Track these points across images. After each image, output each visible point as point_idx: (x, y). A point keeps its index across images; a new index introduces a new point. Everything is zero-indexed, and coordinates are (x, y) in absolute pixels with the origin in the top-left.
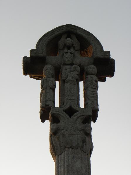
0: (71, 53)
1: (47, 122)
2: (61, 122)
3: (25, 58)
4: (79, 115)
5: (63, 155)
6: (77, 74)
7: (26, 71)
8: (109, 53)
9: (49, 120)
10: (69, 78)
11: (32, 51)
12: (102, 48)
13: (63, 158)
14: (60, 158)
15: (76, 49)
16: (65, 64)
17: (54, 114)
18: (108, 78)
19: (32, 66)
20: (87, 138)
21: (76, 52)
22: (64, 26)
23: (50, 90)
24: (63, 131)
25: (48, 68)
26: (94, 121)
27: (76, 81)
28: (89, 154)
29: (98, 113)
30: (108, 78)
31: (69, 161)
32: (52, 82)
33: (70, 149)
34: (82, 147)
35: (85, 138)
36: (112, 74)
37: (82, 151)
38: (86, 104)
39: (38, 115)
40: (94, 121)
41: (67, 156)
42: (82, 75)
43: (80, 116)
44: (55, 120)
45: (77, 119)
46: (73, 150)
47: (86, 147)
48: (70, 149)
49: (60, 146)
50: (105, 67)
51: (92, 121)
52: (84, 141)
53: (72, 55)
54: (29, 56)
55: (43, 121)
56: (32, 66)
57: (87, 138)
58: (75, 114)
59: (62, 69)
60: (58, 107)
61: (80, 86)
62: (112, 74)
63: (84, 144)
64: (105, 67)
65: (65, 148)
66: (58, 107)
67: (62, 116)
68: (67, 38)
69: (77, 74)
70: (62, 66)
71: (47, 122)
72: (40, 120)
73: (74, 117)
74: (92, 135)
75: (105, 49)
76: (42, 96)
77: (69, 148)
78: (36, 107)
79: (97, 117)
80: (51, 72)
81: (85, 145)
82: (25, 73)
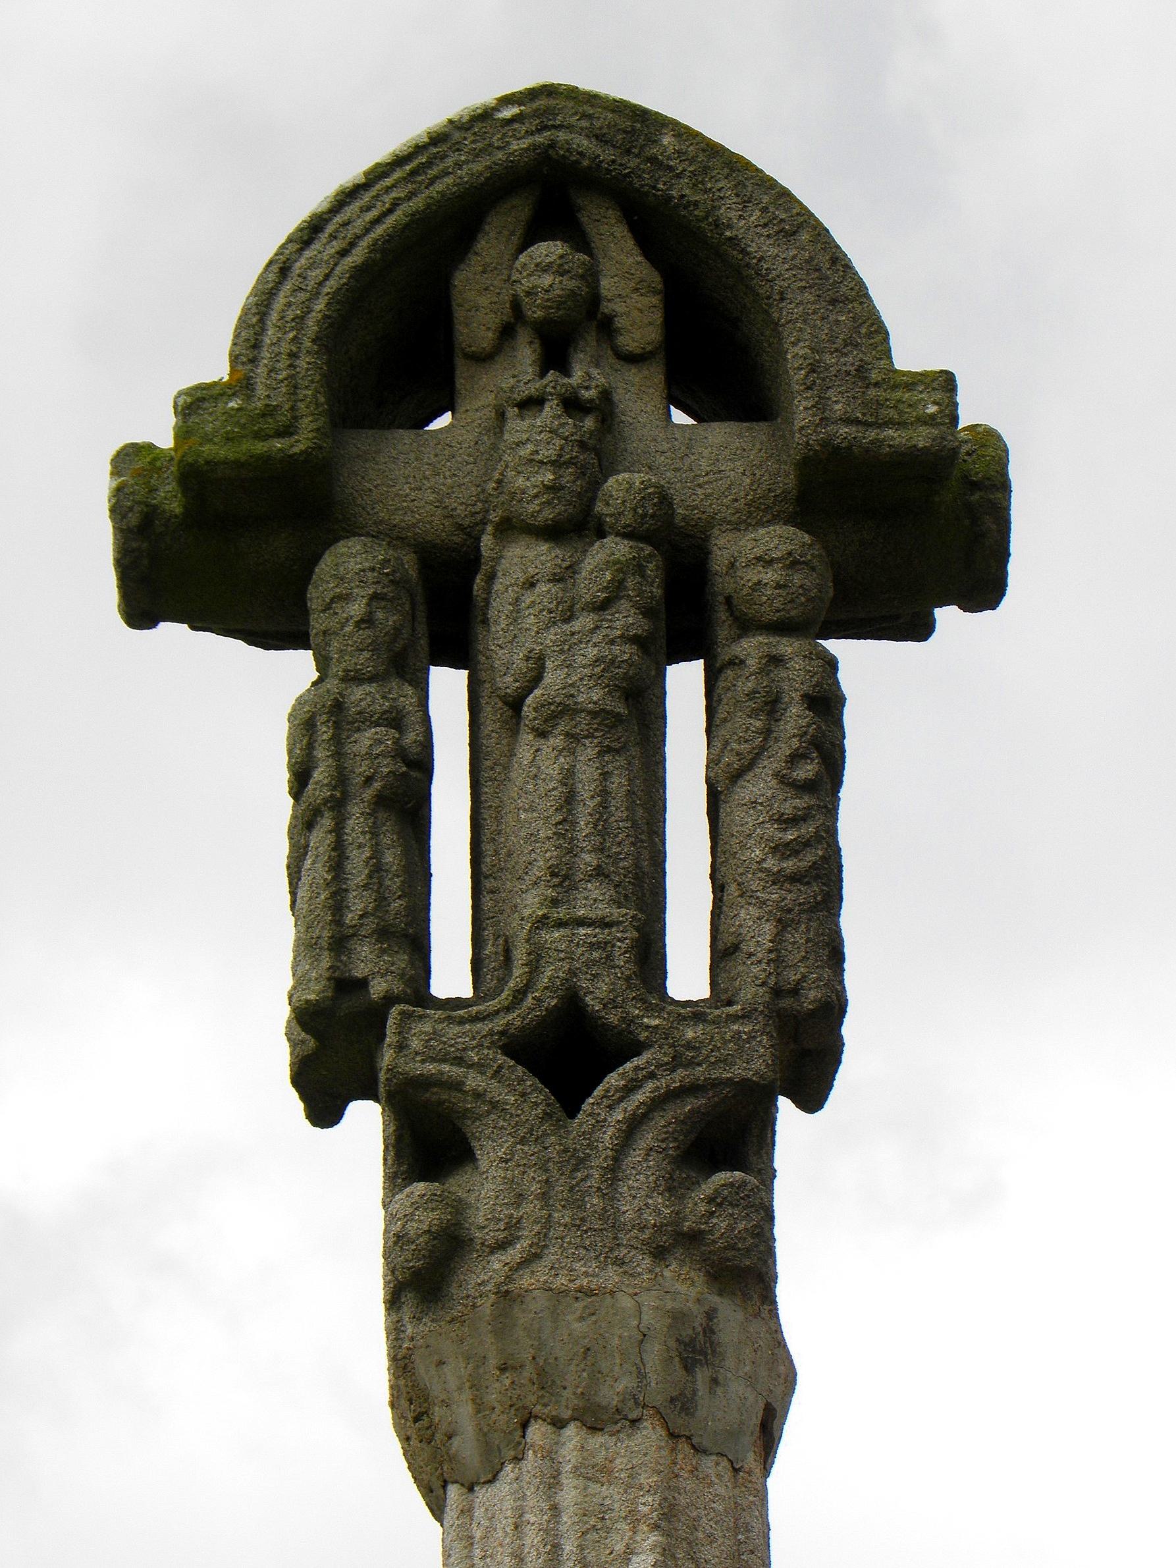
0: (572, 405)
1: (365, 1120)
2: (483, 1164)
3: (132, 460)
4: (650, 1085)
5: (503, 1487)
6: (634, 640)
7: (150, 594)
8: (945, 383)
9: (377, 1100)
10: (553, 678)
11: (194, 404)
12: (874, 332)
13: (505, 1523)
14: (479, 1513)
15: (630, 342)
16: (509, 528)
17: (425, 1083)
18: (947, 617)
19: (204, 539)
20: (766, 1228)
21: (633, 375)
22: (508, 113)
23: (382, 815)
24: (497, 1263)
25: (348, 572)
26: (812, 1097)
27: (621, 709)
28: (751, 1460)
29: (846, 1030)
30: (947, 617)
31: (557, 1547)
32: (388, 736)
33: (571, 1431)
34: (684, 1403)
35: (711, 1315)
36: (983, 587)
37: (683, 1446)
38: (723, 953)
39: (278, 1058)
40: (812, 1097)
41: (545, 1506)
42: (686, 615)
43: (657, 1103)
44: (426, 1147)
45: (616, 1159)
46: (599, 1439)
47: (718, 1390)
48: (571, 1431)
49: (479, 1406)
50: (920, 524)
51: (781, 1098)
52: (696, 1350)
53: (589, 423)
54: (165, 440)
55: (325, 1111)
56: (204, 539)
57: (731, 1317)
58: (613, 1080)
59: (491, 578)
60: (466, 990)
61: (668, 749)
62: (983, 587)
63: (702, 1375)
64: (920, 524)
65: (525, 1426)
66: (466, 990)
67: (494, 1105)
68: (530, 238)
69: (634, 640)
70: (487, 541)
71: (365, 1120)
72: (297, 1106)
73: (608, 1106)
74: (1012, 520)
75: (908, 356)
76: (300, 894)
77: (558, 1424)
78: (250, 970)
79: (839, 1062)
80: (380, 615)
81: (715, 1381)
82: (144, 603)
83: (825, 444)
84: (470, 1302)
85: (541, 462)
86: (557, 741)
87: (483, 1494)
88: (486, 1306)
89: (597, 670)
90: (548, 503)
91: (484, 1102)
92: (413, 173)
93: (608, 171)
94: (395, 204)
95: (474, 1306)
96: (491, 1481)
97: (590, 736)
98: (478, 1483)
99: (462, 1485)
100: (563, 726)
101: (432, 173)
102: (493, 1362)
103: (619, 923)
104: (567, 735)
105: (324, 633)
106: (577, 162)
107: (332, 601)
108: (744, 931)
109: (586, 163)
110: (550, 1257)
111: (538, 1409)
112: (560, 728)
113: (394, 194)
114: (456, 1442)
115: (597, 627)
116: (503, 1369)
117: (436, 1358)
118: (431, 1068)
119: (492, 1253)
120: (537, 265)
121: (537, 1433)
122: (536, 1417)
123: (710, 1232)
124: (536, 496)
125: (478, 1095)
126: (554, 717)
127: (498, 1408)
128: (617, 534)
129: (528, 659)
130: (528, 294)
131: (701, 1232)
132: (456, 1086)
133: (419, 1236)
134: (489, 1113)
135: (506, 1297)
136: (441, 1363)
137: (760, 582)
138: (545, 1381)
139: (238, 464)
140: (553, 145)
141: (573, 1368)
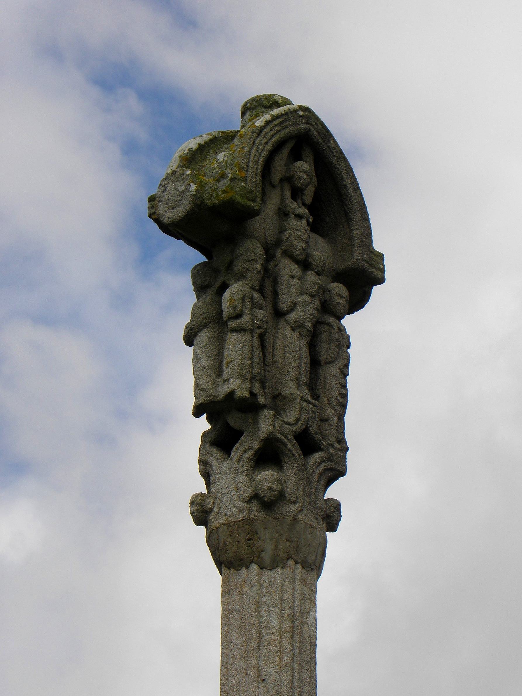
22: (301, 113)
49: (276, 547)
65: (288, 559)
77: (296, 563)
83: (363, 267)
84: (282, 516)
85: (302, 239)
86: (297, 334)
87: (267, 573)
88: (289, 519)
89: (311, 317)
90: (302, 253)
91: (291, 453)
92: (281, 123)
93: (320, 146)
94: (278, 131)
95: (284, 518)
96: (270, 570)
97: (305, 336)
98: (266, 568)
99: (259, 566)
100: (299, 330)
101: (285, 125)
102: (285, 537)
103: (318, 407)
104: (300, 333)
105: (247, 269)
106: (314, 139)
107: (252, 260)
108: (330, 416)
109: (315, 140)
110: (305, 512)
111: (293, 556)
112: (298, 330)
113: (276, 128)
114: (263, 554)
115: (311, 302)
116: (287, 540)
117: (264, 526)
118: (280, 436)
119: (291, 504)
120: (303, 170)
121: (291, 563)
122: (292, 558)
123: (333, 517)
124: (299, 250)
125: (290, 450)
126: (298, 326)
127: (282, 550)
128: (315, 272)
129: (292, 303)
130: (299, 177)
131: (331, 516)
132: (285, 445)
133: (276, 491)
134: (291, 457)
135: (295, 520)
136: (266, 528)
137: (339, 303)
138: (297, 549)
139: (243, 206)
140: (310, 130)
141: (305, 548)
